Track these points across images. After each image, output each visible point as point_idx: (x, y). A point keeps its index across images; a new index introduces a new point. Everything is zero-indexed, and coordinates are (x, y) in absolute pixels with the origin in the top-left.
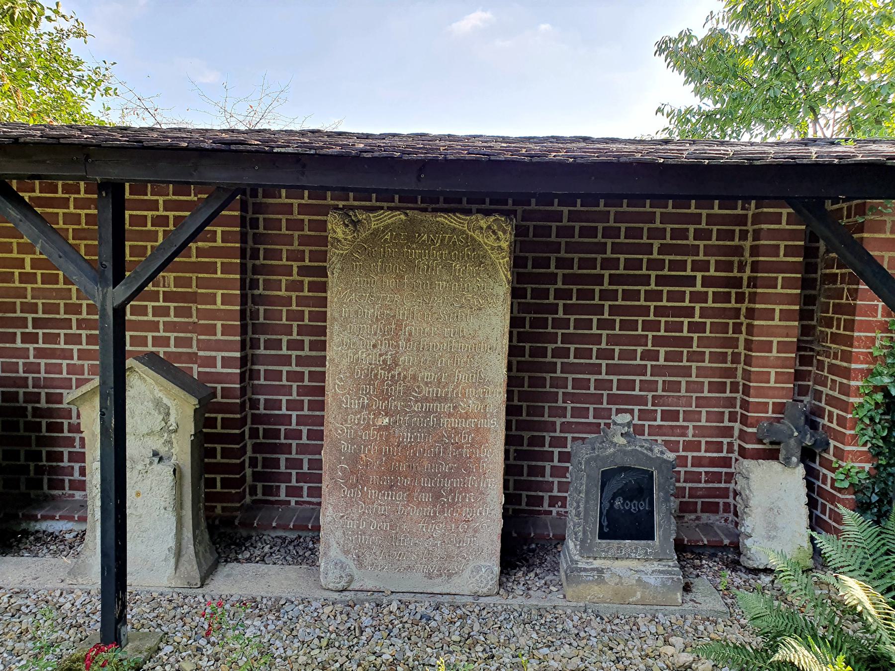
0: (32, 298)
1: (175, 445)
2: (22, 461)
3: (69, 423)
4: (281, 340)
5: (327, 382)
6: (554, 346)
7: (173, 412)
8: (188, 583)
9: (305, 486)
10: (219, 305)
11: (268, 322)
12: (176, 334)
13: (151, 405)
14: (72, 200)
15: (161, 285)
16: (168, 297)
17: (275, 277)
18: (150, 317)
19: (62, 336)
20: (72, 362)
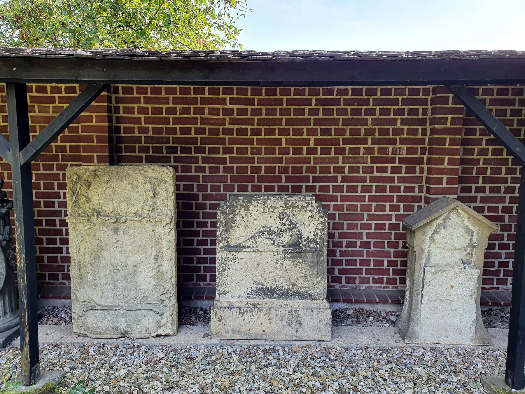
0: (314, 164)
1: (474, 255)
2: (496, 268)
3: (333, 241)
4: (471, 187)
5: (68, 208)
6: (506, 186)
7: (475, 234)
8: (483, 342)
9: (344, 276)
10: (446, 166)
11: (464, 175)
12: (405, 184)
13: (463, 230)
14: (342, 99)
15: (398, 153)
16: (402, 161)
17: (471, 147)
18: (389, 174)
19: (331, 187)
20: (337, 203)
